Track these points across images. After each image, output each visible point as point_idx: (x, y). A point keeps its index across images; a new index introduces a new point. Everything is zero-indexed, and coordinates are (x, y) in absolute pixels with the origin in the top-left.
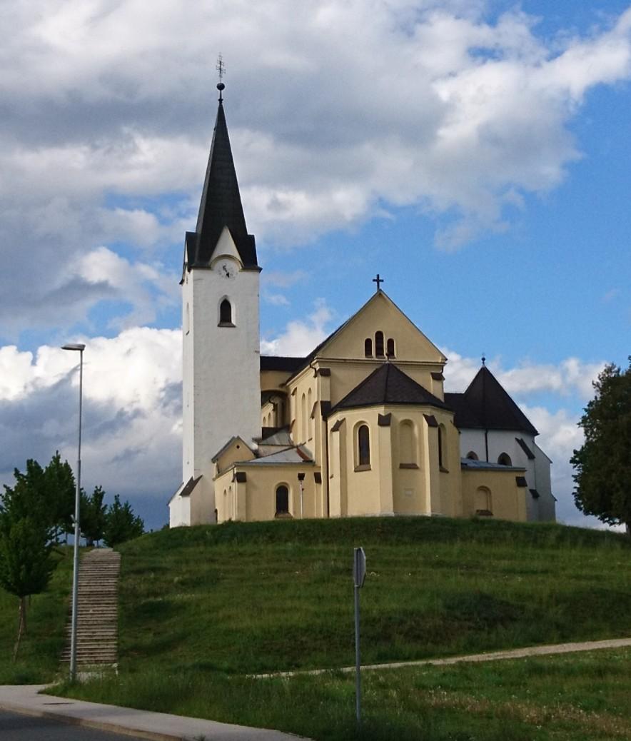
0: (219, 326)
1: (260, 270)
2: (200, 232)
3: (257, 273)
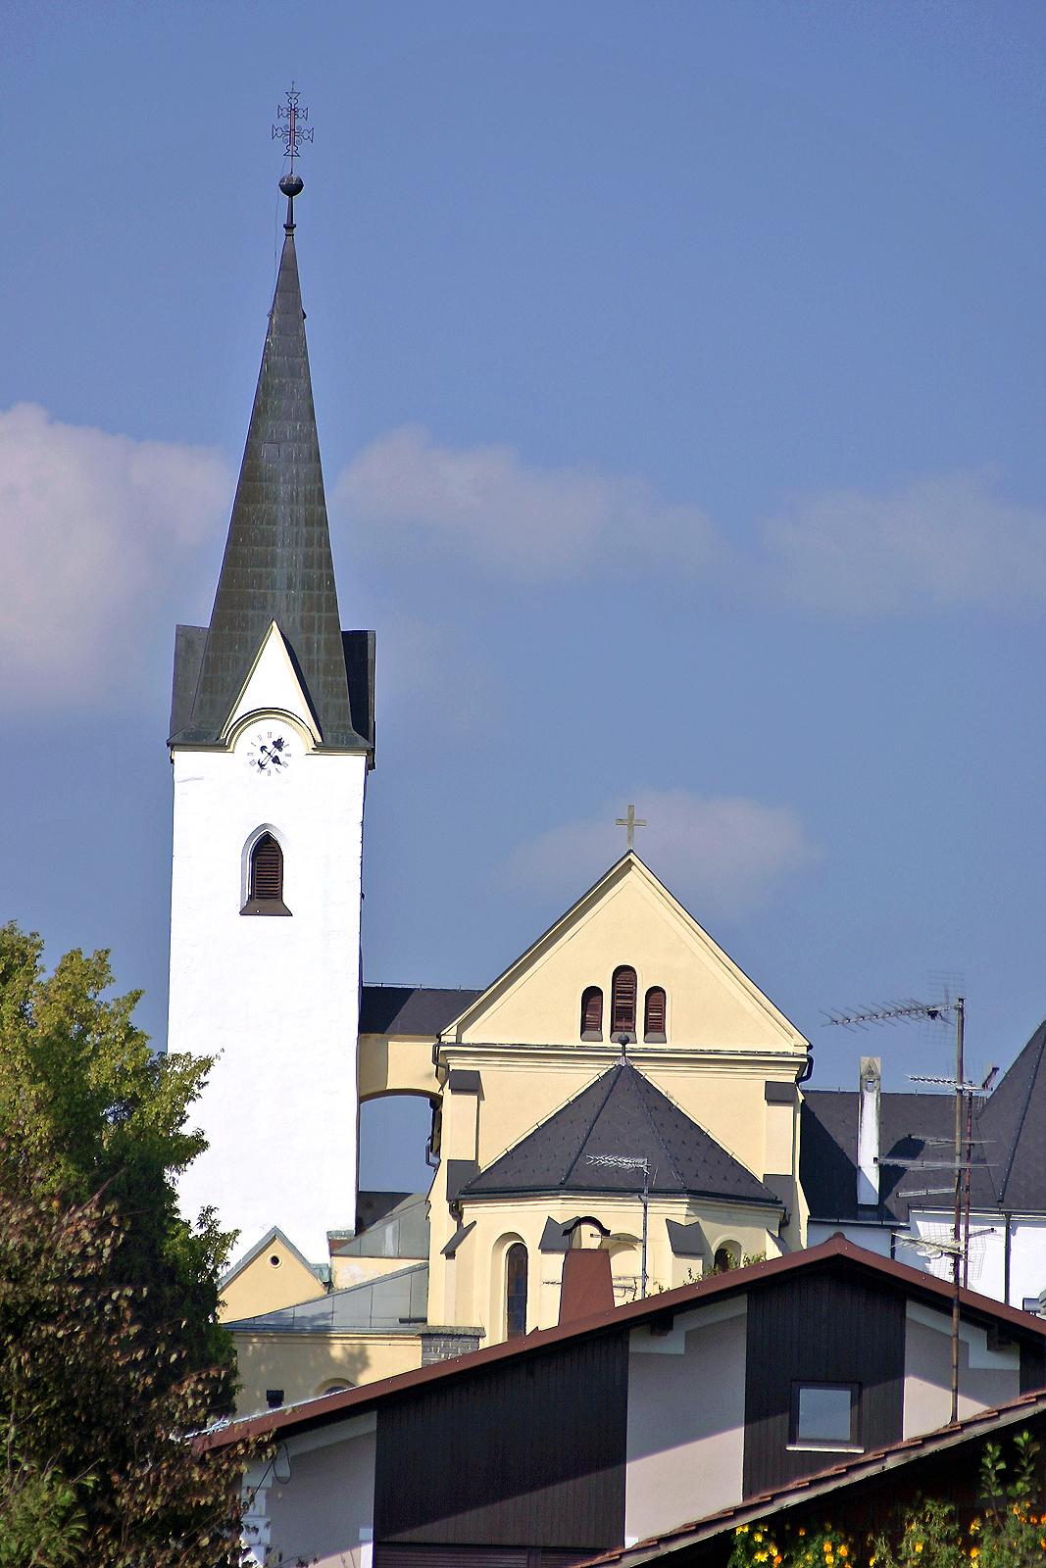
0: (243, 913)
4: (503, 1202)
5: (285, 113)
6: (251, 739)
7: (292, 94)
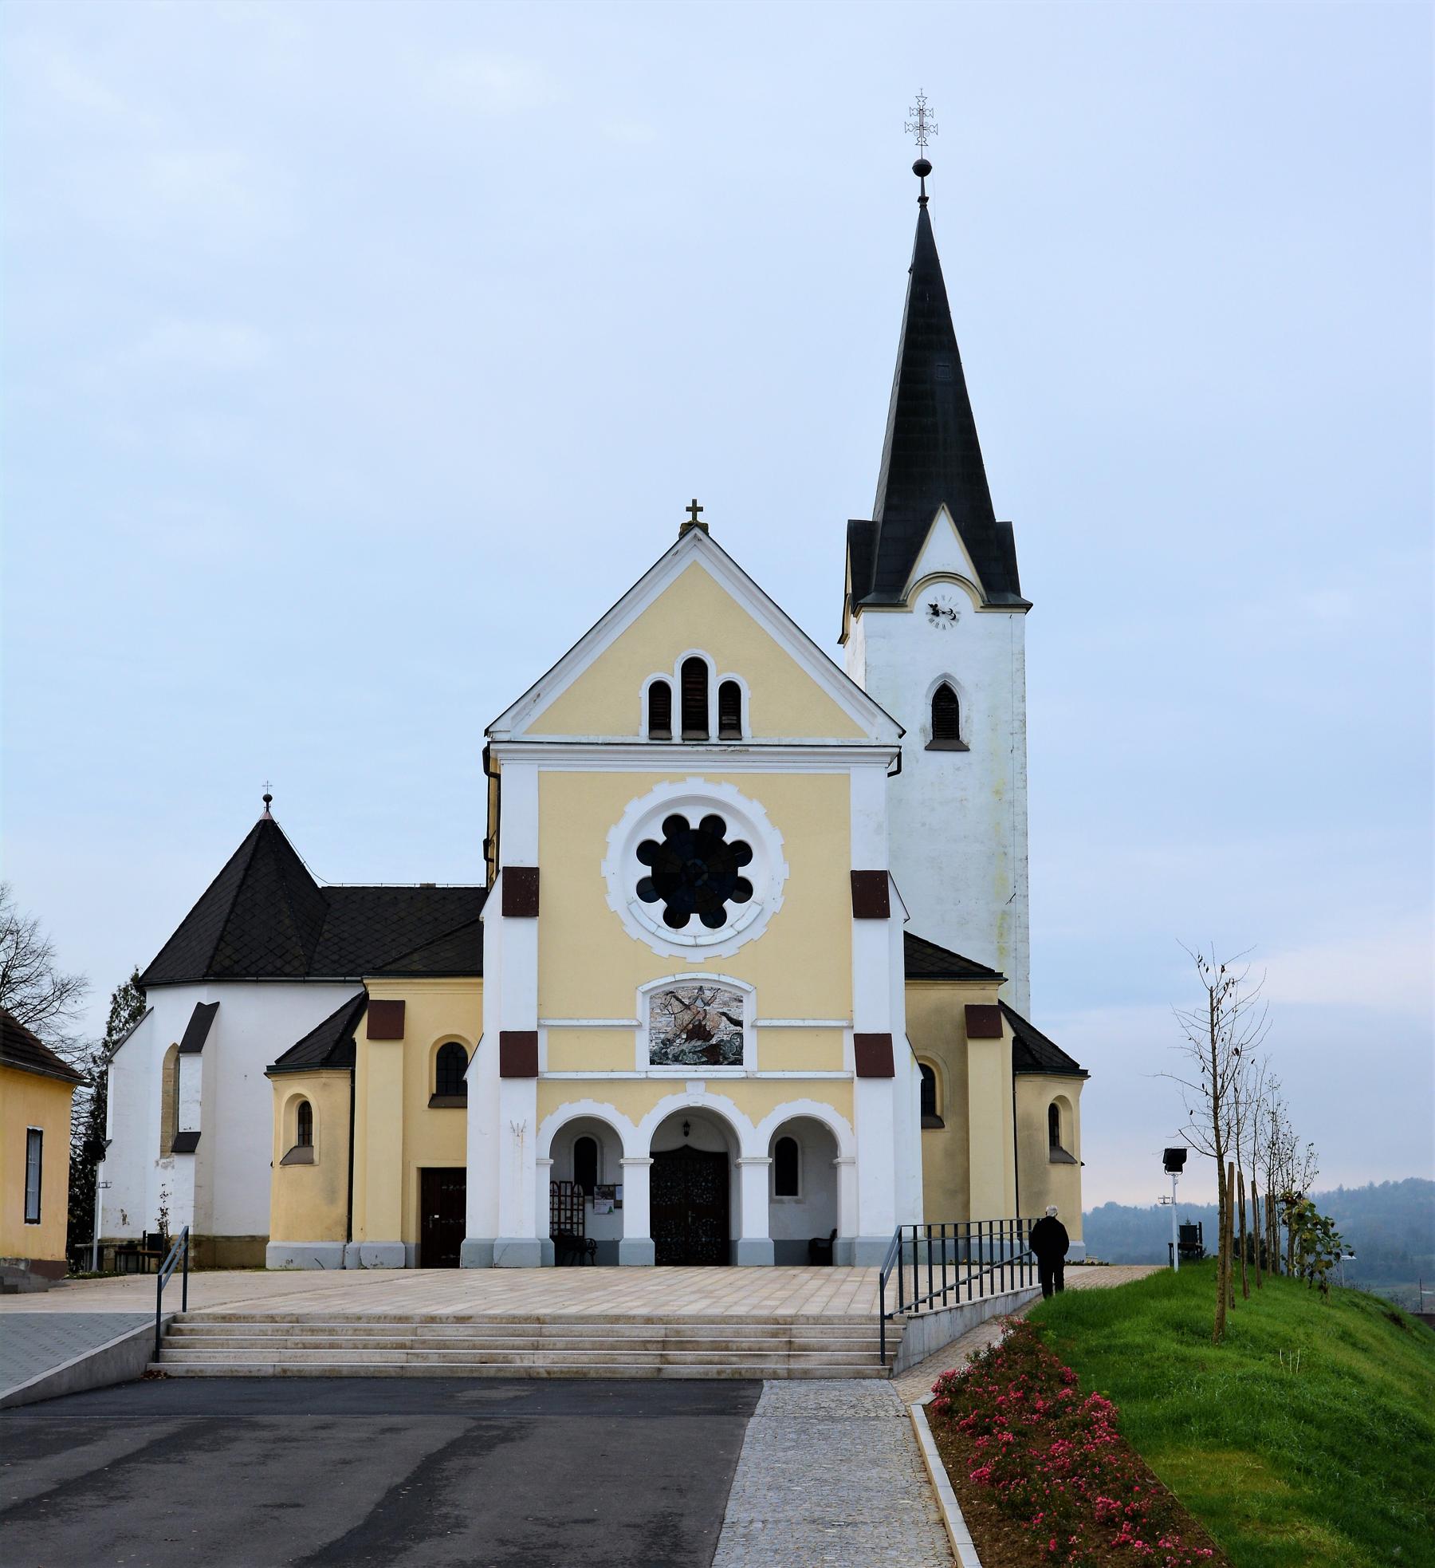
0: (927, 748)
1: (1028, 606)
2: (879, 519)
3: (1017, 616)
4: (926, 980)
5: (915, 112)
6: (921, 600)
7: (921, 98)
